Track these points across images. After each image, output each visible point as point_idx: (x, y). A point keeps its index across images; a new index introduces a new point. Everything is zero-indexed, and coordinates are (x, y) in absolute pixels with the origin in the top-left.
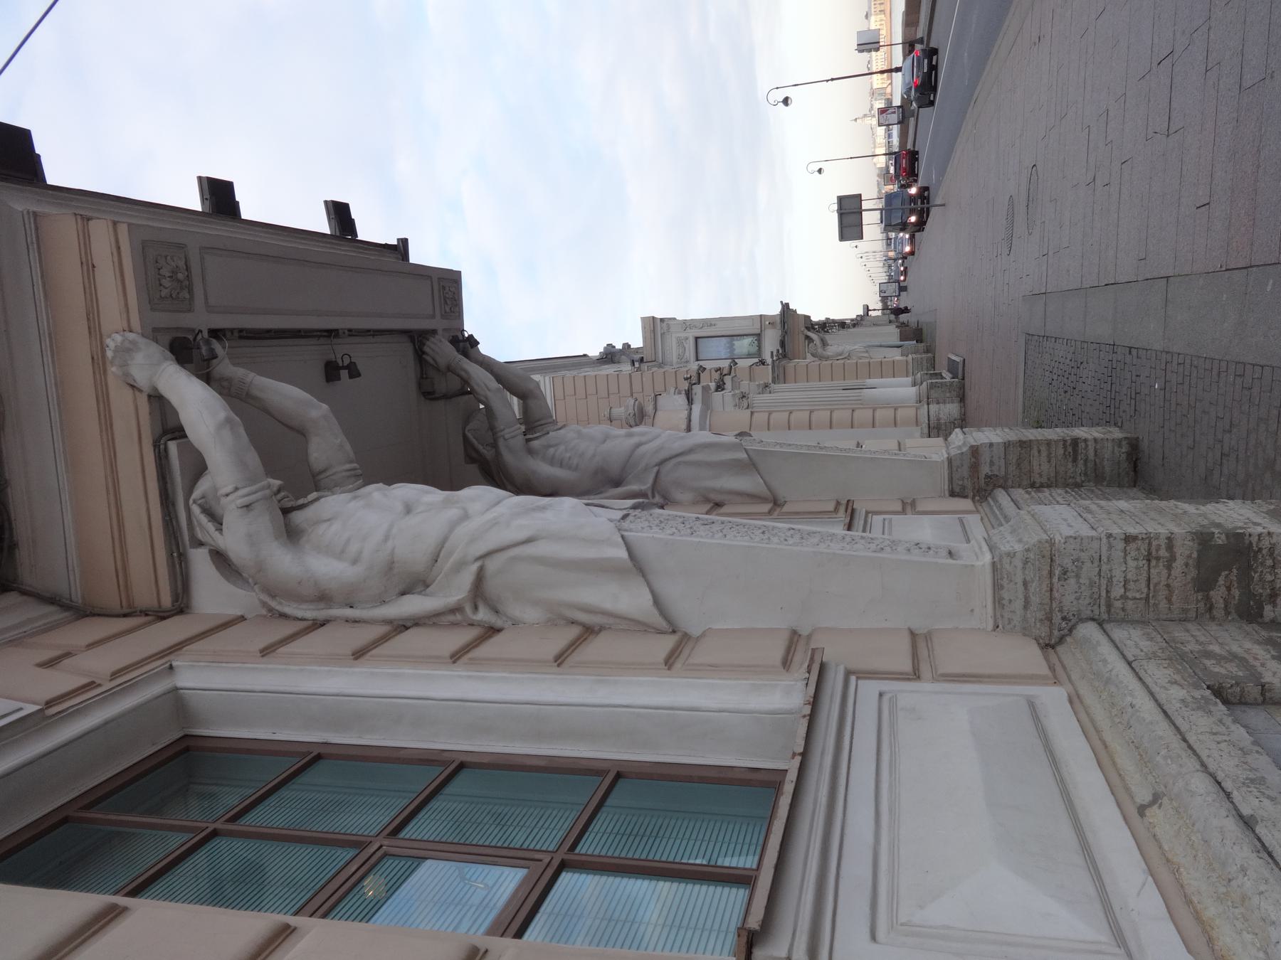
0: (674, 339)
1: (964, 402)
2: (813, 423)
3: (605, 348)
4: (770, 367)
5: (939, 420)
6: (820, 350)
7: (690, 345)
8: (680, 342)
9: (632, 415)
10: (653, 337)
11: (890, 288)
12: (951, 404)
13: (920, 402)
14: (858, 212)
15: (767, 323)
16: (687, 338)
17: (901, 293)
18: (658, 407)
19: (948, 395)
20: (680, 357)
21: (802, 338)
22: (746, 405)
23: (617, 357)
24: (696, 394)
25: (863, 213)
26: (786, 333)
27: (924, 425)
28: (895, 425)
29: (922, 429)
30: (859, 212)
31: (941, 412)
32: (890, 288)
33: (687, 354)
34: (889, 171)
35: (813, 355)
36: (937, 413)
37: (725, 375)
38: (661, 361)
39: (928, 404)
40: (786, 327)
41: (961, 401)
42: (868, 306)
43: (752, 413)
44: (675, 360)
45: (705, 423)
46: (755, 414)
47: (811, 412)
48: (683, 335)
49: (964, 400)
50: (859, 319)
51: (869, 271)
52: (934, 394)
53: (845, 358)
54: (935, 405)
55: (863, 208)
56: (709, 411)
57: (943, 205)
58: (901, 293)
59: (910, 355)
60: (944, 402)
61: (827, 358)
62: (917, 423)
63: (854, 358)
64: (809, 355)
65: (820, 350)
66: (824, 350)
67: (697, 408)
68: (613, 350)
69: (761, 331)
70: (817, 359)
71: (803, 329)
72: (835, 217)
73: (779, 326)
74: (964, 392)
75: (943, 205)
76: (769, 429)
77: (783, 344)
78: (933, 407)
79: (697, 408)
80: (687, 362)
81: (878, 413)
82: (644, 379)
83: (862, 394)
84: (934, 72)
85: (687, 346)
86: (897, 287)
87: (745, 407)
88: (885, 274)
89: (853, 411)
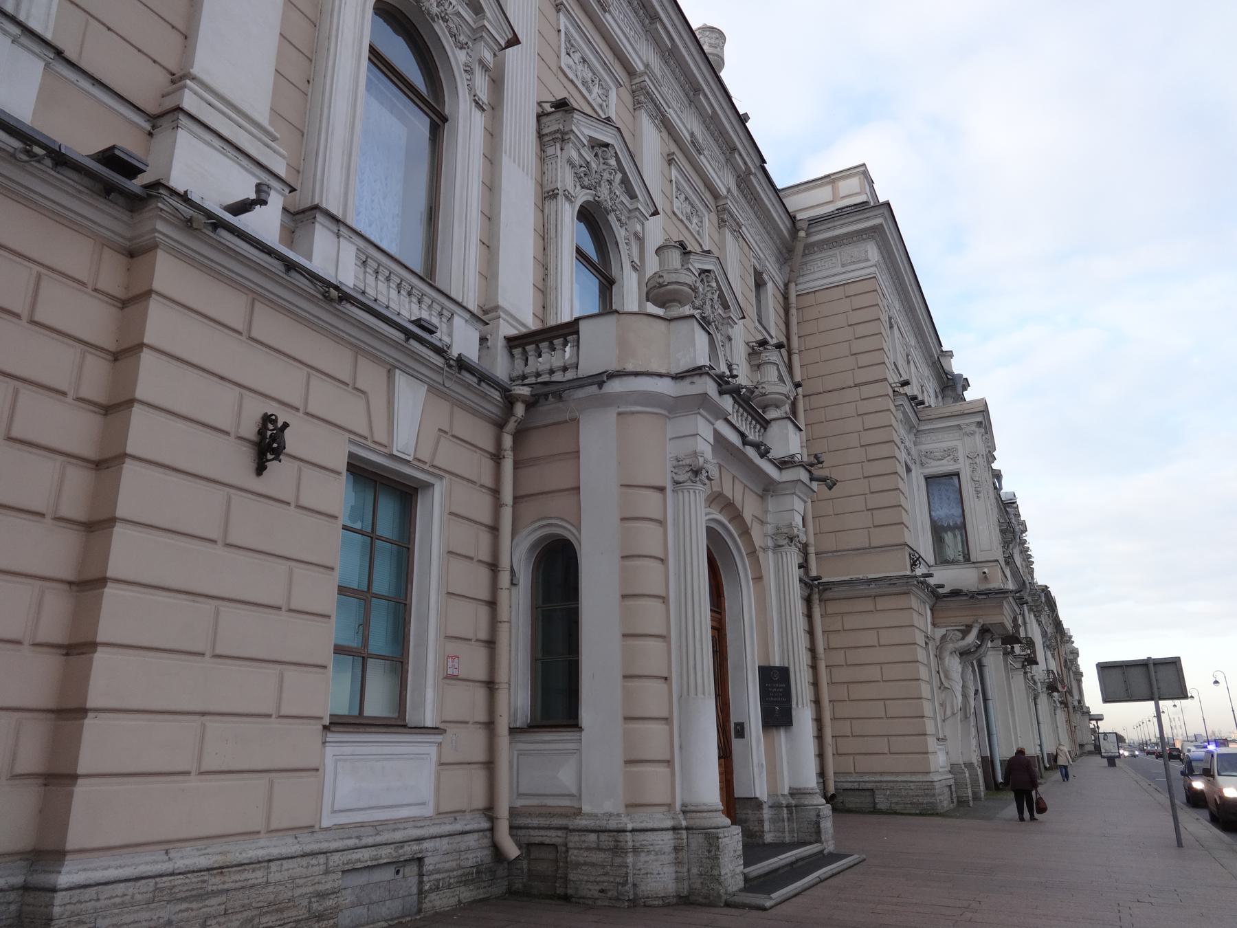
0: (955, 443)
1: (677, 904)
2: (631, 602)
3: (961, 376)
4: (908, 573)
5: (636, 851)
6: (951, 646)
7: (946, 467)
8: (949, 453)
9: (661, 280)
10: (954, 414)
11: (1112, 746)
12: (674, 876)
13: (684, 812)
14: (1152, 694)
15: (986, 570)
16: (956, 460)
17: (1106, 760)
18: (673, 324)
19: (695, 871)
20: (928, 455)
21: (968, 620)
22: (680, 478)
23: (950, 393)
24: (692, 383)
25: (1152, 704)
26: (972, 598)
27: (625, 820)
28: (629, 762)
29: (618, 815)
30: (1154, 695)
31: (652, 857)
32: (1112, 746)
33: (934, 463)
34: (788, 810)
35: (944, 637)
36: (651, 848)
37: (810, 472)
38: (920, 428)
39: (674, 829)
40: (980, 597)
41: (679, 897)
42: (1102, 719)
43: (662, 489)
44: (923, 447)
45: (636, 403)
46: (656, 496)
47: (663, 598)
48: (961, 455)
49: (685, 904)
50: (1085, 710)
51: (1149, 721)
52: (697, 840)
53: (942, 683)
54: (672, 843)
55: (1161, 703)
56: (665, 413)
57: (1180, 844)
58: (1106, 760)
59: (951, 776)
60: (678, 863)
61: (939, 657)
62: (632, 806)
63: (943, 695)
64: (942, 631)
65: (951, 646)
66: (951, 653)
67: (665, 387)
68: (960, 389)
69: (973, 563)
70: (938, 643)
71: (981, 621)
72: (1142, 656)
73: (983, 587)
74: (701, 905)
75: (1180, 844)
76: (623, 519)
77: (956, 593)
78: (665, 841)
79: (665, 387)
80: (922, 464)
81: (658, 728)
82: (880, 399)
83: (806, 707)
84: (701, 97)
85: (945, 462)
86: (1113, 755)
87: (677, 478)
88: (1144, 740)
89: (666, 679)
